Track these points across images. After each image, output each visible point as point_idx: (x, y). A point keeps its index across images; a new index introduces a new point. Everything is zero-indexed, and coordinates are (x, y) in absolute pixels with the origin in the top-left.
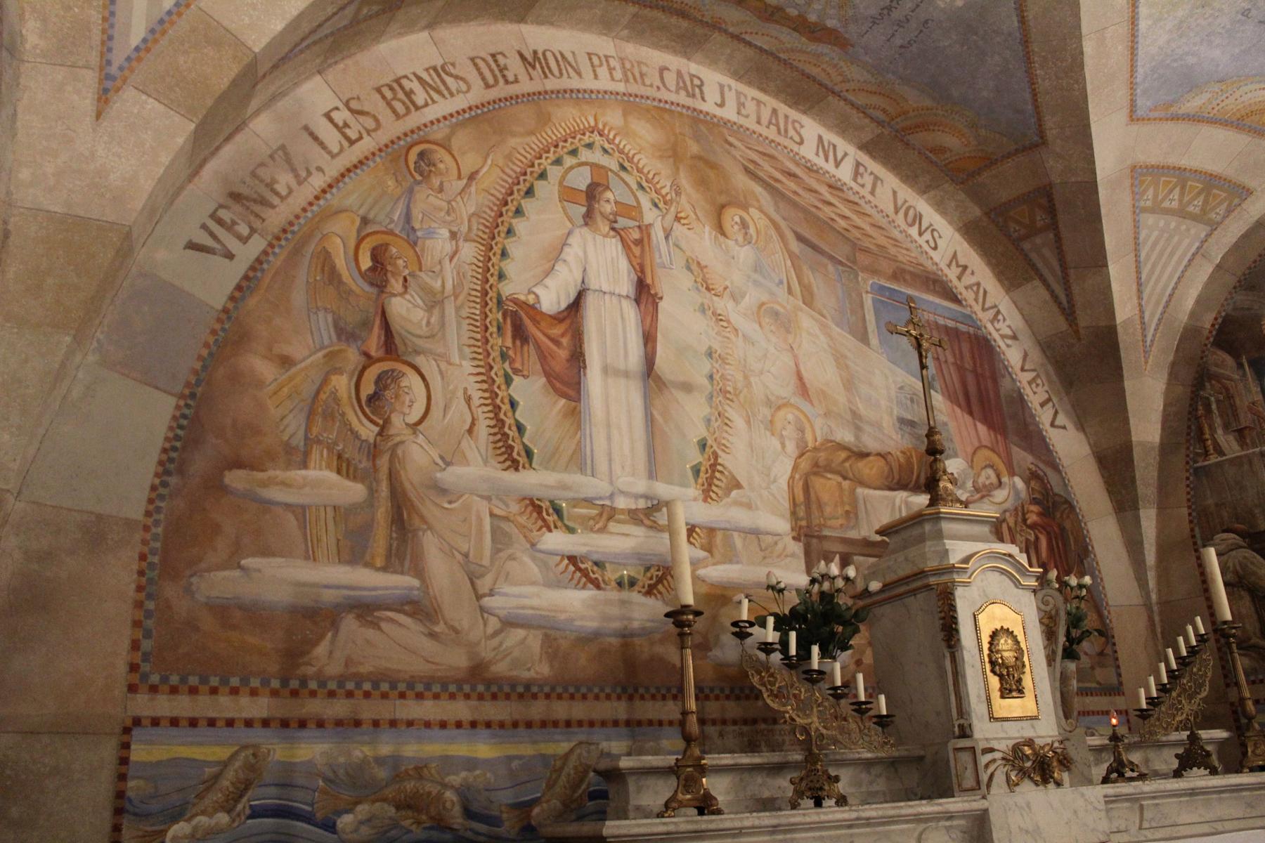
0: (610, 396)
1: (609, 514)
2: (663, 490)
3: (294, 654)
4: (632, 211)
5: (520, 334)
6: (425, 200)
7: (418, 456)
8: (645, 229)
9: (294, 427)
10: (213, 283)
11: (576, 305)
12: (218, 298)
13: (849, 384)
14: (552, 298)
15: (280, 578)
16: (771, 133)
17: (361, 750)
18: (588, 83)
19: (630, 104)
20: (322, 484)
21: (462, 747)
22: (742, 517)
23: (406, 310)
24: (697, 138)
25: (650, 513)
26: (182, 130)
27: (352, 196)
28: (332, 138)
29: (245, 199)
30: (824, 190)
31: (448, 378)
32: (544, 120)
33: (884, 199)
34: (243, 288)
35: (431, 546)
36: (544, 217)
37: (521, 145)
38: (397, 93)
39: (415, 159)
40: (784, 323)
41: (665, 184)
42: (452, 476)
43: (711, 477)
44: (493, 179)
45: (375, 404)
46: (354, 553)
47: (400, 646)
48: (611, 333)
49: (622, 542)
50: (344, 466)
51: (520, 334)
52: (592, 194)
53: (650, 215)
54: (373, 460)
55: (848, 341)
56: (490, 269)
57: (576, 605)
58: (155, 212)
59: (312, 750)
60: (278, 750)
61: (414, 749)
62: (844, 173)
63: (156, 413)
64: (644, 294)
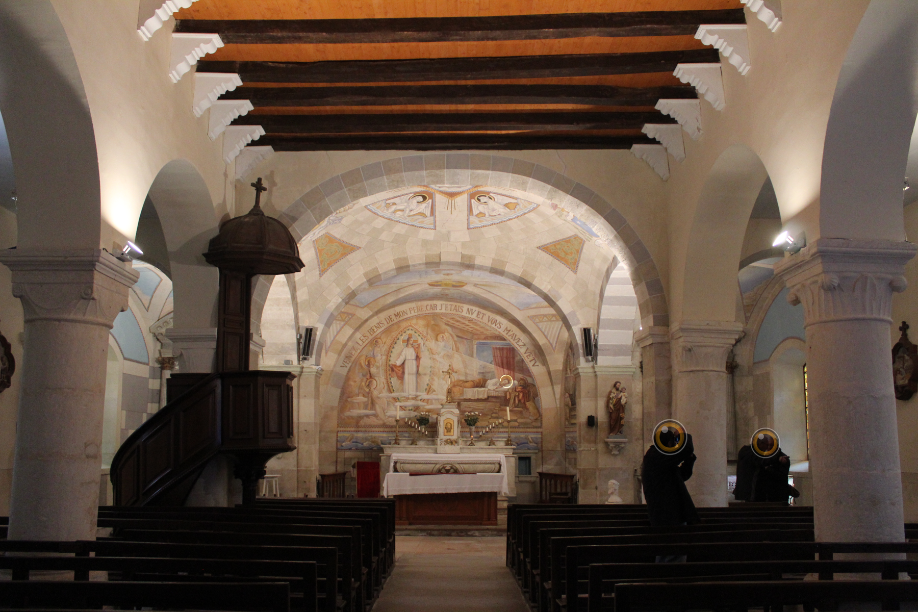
0: (409, 379)
1: (408, 399)
2: (418, 394)
3: (358, 422)
4: (416, 341)
5: (393, 370)
6: (377, 349)
7: (375, 393)
8: (419, 345)
9: (357, 391)
10: (344, 371)
11: (403, 363)
12: (345, 374)
13: (465, 367)
14: (399, 363)
15: (355, 412)
16: (454, 312)
17: (367, 435)
18: (409, 315)
19: (418, 317)
20: (361, 399)
21: (381, 435)
22: (435, 397)
23: (373, 370)
24: (434, 320)
25: (415, 398)
26: (336, 356)
27: (364, 352)
28: (360, 342)
29: (348, 357)
30: (467, 323)
31: (380, 380)
32: (399, 327)
33: (485, 319)
34: (349, 371)
35: (377, 407)
36: (400, 345)
37: (394, 334)
38: (372, 330)
39: (375, 342)
40: (449, 357)
41: (425, 334)
42: (380, 396)
43: (429, 390)
44: (389, 341)
45: (369, 386)
46: (366, 408)
47: (373, 421)
48: (411, 367)
49: (410, 403)
50: (364, 396)
51: (393, 370)
52: (408, 340)
53: (420, 341)
54: (368, 394)
55: (467, 358)
56: (388, 360)
57: (400, 414)
58: (335, 365)
59: (360, 435)
60: (356, 435)
61: (374, 435)
62: (474, 316)
63: (338, 392)
64: (418, 358)
